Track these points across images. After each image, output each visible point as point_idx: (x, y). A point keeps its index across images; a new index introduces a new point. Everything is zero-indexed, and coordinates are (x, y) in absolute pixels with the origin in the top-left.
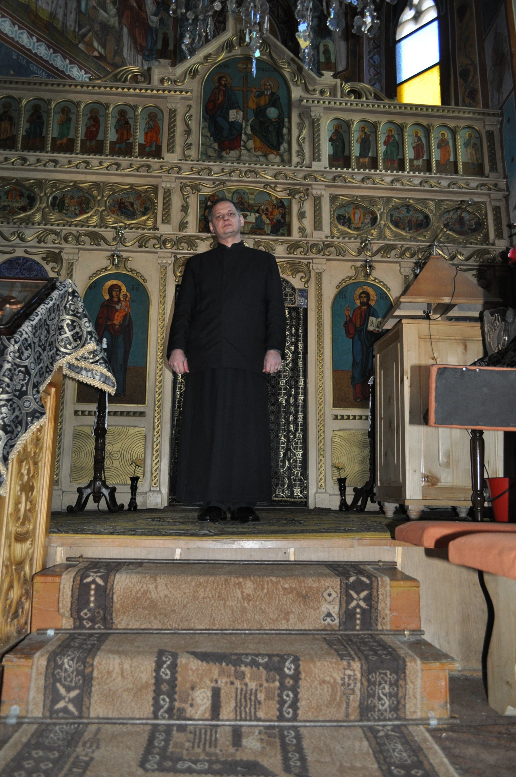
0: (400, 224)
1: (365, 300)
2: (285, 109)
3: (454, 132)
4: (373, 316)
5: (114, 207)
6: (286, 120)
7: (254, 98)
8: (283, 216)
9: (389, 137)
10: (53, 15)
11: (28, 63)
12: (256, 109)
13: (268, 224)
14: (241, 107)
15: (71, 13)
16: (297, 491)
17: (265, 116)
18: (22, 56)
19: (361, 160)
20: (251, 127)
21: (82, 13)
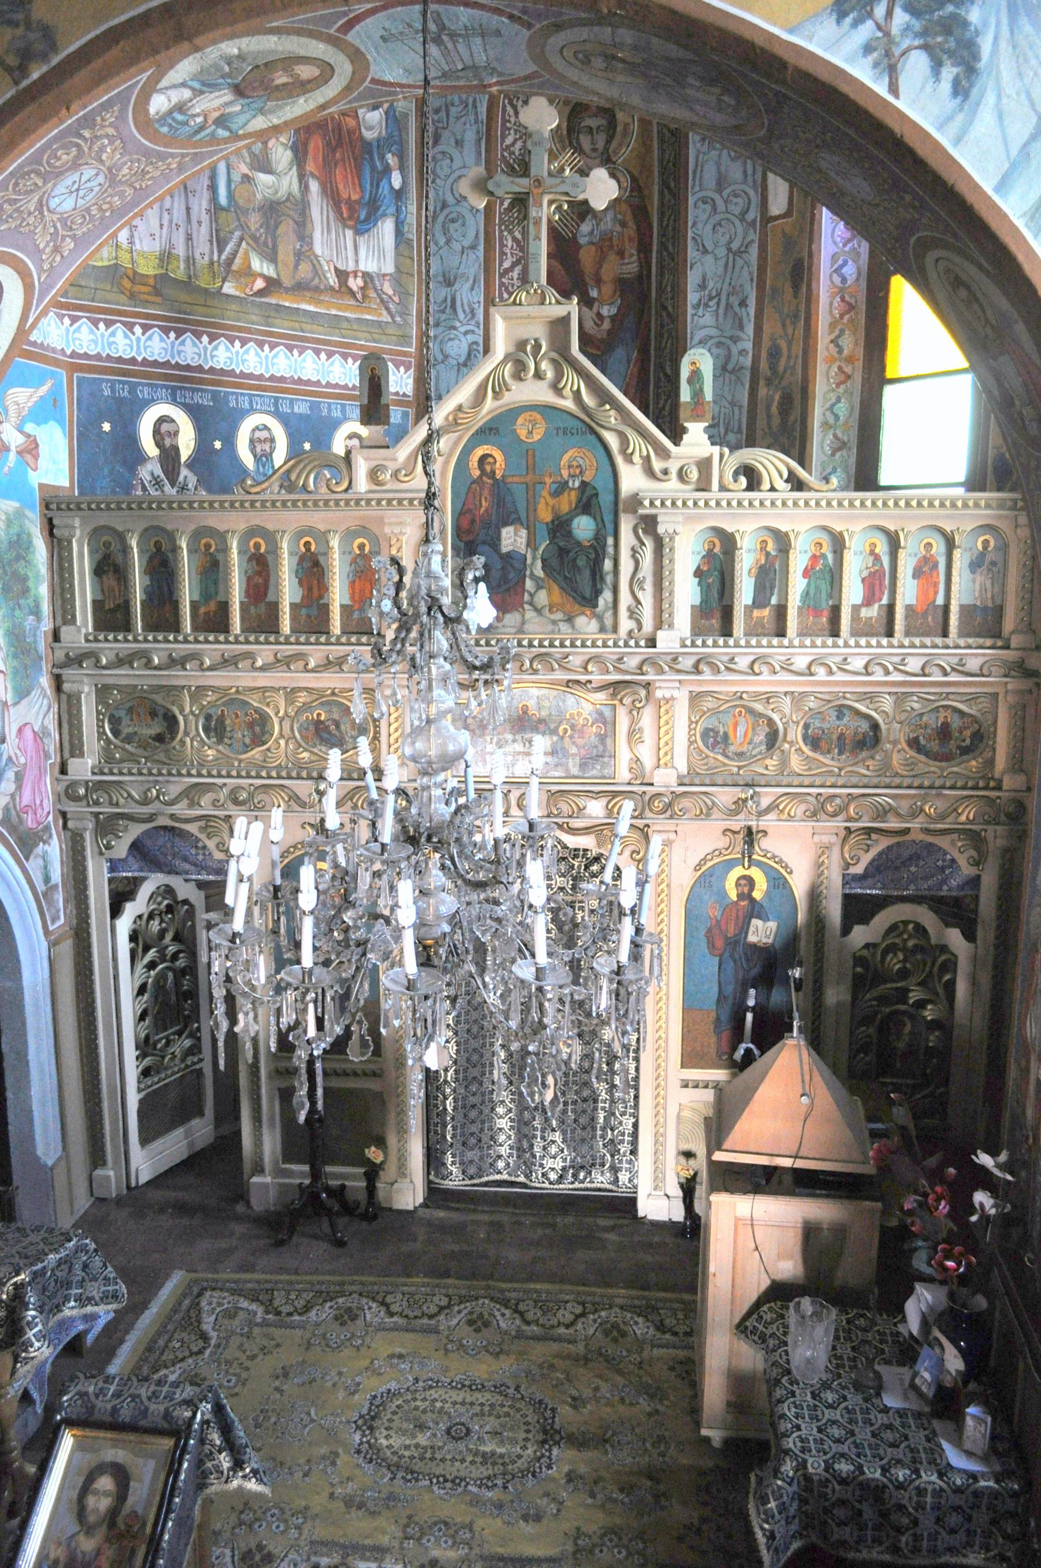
0: (823, 744)
1: (746, 890)
2: (608, 518)
3: (950, 544)
4: (759, 917)
5: (307, 729)
6: (610, 541)
7: (548, 498)
8: (602, 738)
9: (814, 558)
10: (166, 257)
11: (133, 387)
12: (553, 521)
13: (574, 755)
14: (524, 519)
15: (200, 223)
16: (624, 1177)
17: (569, 534)
18: (120, 382)
19: (756, 613)
20: (543, 561)
21: (223, 209)
